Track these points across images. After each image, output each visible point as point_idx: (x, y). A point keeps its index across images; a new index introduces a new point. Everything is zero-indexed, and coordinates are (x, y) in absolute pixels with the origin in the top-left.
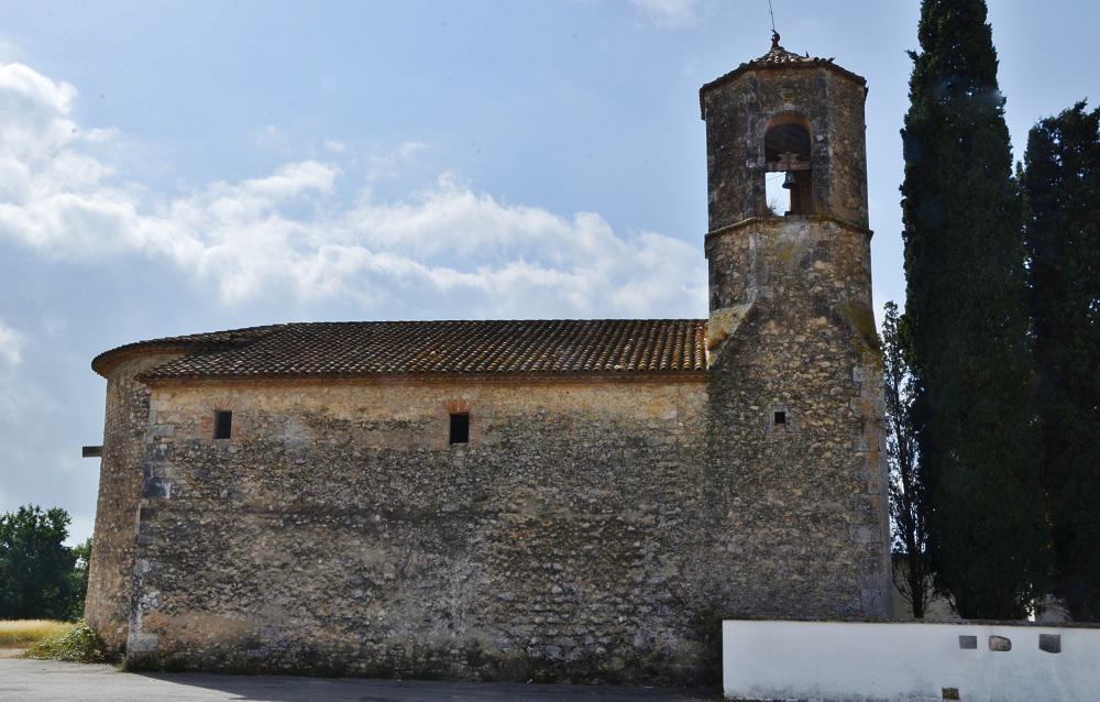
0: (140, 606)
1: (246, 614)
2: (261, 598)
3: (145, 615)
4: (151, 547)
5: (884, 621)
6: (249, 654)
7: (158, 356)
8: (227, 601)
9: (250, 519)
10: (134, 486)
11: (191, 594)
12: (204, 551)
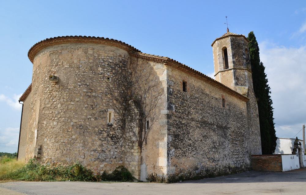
0: (170, 155)
1: (194, 157)
2: (197, 152)
3: (171, 159)
4: (171, 131)
5: (281, 163)
6: (197, 172)
7: (115, 47)
8: (191, 153)
9: (193, 123)
10: (104, 101)
11: (182, 151)
12: (184, 134)
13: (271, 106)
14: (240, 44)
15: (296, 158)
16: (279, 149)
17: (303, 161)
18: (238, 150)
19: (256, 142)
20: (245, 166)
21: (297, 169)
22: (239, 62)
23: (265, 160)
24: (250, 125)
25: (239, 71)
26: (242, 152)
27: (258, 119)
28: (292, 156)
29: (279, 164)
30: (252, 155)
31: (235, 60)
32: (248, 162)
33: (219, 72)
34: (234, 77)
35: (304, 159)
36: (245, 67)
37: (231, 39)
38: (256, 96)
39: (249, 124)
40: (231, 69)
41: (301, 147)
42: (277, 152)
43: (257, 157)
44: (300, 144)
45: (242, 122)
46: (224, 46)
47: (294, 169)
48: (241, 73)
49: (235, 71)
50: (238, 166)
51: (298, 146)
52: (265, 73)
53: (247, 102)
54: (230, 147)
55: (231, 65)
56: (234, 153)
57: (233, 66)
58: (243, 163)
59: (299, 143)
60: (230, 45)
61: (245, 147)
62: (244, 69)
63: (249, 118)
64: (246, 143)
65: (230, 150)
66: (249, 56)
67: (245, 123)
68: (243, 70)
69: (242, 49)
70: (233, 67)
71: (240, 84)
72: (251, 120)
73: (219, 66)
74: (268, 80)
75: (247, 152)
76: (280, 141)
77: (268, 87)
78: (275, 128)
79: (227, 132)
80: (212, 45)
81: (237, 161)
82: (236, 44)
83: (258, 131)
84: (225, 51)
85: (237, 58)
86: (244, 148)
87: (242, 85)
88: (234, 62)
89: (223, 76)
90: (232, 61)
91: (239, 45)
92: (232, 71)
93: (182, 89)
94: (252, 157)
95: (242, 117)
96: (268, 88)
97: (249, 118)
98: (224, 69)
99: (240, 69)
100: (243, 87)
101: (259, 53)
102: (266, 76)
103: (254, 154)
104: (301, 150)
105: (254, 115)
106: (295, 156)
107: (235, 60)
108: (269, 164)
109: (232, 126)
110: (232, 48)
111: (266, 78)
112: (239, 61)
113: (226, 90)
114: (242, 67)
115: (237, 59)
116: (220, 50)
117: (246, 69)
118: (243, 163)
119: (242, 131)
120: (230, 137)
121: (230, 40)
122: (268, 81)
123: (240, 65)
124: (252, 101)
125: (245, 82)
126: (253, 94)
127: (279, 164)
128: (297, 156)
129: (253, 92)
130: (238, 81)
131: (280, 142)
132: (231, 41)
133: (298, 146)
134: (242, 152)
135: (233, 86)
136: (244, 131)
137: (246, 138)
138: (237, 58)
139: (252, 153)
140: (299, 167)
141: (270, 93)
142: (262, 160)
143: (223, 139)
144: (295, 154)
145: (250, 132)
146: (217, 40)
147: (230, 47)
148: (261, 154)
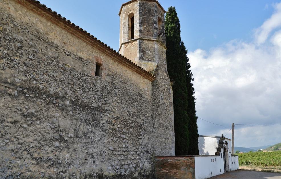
5: (194, 168)
13: (193, 95)
14: (151, 10)
15: (220, 160)
16: (203, 150)
17: (230, 164)
18: (127, 147)
19: (165, 139)
20: (140, 173)
21: (220, 175)
22: (147, 31)
23: (172, 164)
24: (155, 114)
25: (146, 42)
26: (136, 152)
27: (172, 108)
28: (214, 158)
29: (191, 170)
30: (156, 157)
31: (142, 28)
32: (148, 166)
33: (122, 44)
34: (140, 49)
35: (230, 161)
36: (156, 39)
37: (139, 3)
38: (170, 79)
39: (153, 113)
40: (136, 40)
41: (227, 147)
42: (201, 153)
43: (162, 159)
44: (226, 143)
45: (139, 108)
46: (131, 12)
47: (215, 175)
48: (150, 46)
49: (141, 41)
50: (123, 173)
51: (224, 145)
52: (187, 58)
53: (153, 82)
54: (106, 141)
55: (137, 35)
56: (115, 152)
57: (139, 35)
58: (135, 168)
59: (224, 142)
60: (138, 10)
61: (141, 145)
62: (153, 41)
63: (155, 104)
64: (146, 138)
65: (104, 147)
66: (164, 28)
67: (145, 110)
68: (152, 42)
69: (153, 16)
70: (139, 36)
71: (147, 59)
72: (157, 108)
73: (122, 37)
74: (191, 65)
75: (147, 151)
76: (204, 140)
77: (190, 72)
78: (197, 123)
79: (101, 117)
80: (120, 15)
81: (122, 165)
82: (145, 10)
83: (171, 125)
84: (131, 18)
85: (145, 26)
86: (140, 145)
87: (149, 60)
88: (140, 31)
89: (126, 49)
90: (138, 29)
91: (149, 12)
92: (138, 41)
93: (93, 73)
94: (154, 159)
95: (141, 99)
96: (190, 74)
97: (155, 104)
98: (129, 40)
99: (149, 40)
100: (150, 63)
101: (180, 31)
102: (188, 60)
103: (160, 155)
104: (227, 150)
105: (165, 102)
106: (219, 158)
107: (142, 28)
108: (178, 169)
109: (115, 109)
110: (139, 13)
111: (188, 63)
112: (148, 31)
113: (115, 57)
114: (152, 38)
115: (145, 28)
116: (126, 17)
117: (156, 41)
118: (135, 168)
119: (139, 120)
120: (106, 125)
121: (139, 4)
122: (190, 66)
123: (148, 35)
124: (163, 84)
125: (154, 57)
126: (166, 74)
127: (191, 170)
128: (222, 157)
129: (166, 72)
130: (144, 55)
131: (205, 141)
132: (139, 6)
133: (224, 145)
134: (136, 152)
135: (137, 61)
136: (142, 120)
137: (145, 131)
138: (145, 26)
139: (157, 153)
140: (223, 171)
141: (193, 80)
142: (168, 164)
143: (88, 127)
144: (219, 155)
145: (156, 124)
146: (124, 5)
147: (138, 12)
148: (174, 154)
